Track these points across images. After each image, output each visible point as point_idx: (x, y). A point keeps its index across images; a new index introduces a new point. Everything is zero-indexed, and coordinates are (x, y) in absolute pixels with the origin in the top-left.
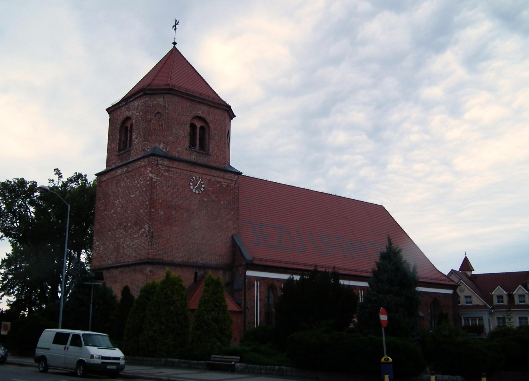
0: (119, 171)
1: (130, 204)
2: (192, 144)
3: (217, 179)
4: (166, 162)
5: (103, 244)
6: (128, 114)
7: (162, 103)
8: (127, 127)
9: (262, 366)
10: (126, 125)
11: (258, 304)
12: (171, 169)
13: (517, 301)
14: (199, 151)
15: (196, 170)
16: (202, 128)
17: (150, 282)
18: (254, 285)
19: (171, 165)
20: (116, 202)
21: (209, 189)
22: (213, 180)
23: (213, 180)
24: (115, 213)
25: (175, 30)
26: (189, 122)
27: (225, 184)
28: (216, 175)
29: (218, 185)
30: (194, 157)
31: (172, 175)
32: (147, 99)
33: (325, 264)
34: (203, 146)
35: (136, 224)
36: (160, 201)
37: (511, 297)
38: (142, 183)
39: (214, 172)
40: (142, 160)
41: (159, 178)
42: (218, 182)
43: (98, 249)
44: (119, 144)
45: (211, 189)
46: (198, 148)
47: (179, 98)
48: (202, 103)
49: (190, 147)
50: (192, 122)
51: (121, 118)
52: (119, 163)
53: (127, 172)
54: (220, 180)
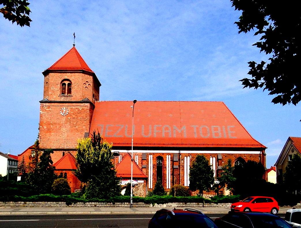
2: (63, 93)
4: (47, 104)
15: (64, 105)
19: (50, 105)
21: (72, 112)
23: (73, 108)
29: (77, 110)
30: (62, 99)
36: (45, 122)
39: (74, 104)
41: (44, 112)
42: (77, 108)
54: (78, 107)
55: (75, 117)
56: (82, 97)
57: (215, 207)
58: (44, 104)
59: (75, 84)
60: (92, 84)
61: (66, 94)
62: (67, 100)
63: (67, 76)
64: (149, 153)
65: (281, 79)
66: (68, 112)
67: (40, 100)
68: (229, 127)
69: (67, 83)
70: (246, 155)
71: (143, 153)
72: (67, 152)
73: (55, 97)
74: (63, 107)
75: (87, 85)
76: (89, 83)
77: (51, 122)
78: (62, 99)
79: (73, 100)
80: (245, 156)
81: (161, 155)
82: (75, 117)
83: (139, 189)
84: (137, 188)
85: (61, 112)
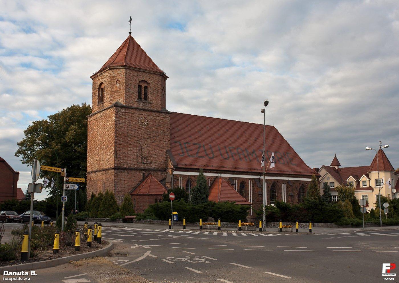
0: (99, 115)
1: (105, 135)
2: (139, 97)
3: (156, 118)
4: (123, 110)
5: (92, 158)
6: (102, 80)
7: (41, 147)
8: (102, 88)
10: (101, 87)
11: (277, 176)
12: (127, 114)
13: (361, 185)
16: (146, 87)
18: (179, 180)
20: (98, 134)
21: (151, 124)
22: (153, 118)
23: (153, 118)
24: (98, 140)
25: (130, 24)
26: (137, 84)
27: (161, 120)
30: (140, 106)
32: (111, 72)
34: (146, 98)
35: (108, 146)
36: (121, 133)
37: (358, 182)
38: (110, 122)
40: (110, 109)
43: (90, 161)
44: (99, 99)
45: (152, 124)
46: (143, 99)
47: (130, 70)
48: (145, 72)
49: (138, 99)
50: (139, 84)
51: (99, 83)
52: (98, 110)
53: (102, 116)
54: (158, 118)
55: (156, 130)
65: (385, 267)
71: (229, 178)
73: (132, 101)
74: (142, 116)
82: (156, 130)
85: (139, 121)
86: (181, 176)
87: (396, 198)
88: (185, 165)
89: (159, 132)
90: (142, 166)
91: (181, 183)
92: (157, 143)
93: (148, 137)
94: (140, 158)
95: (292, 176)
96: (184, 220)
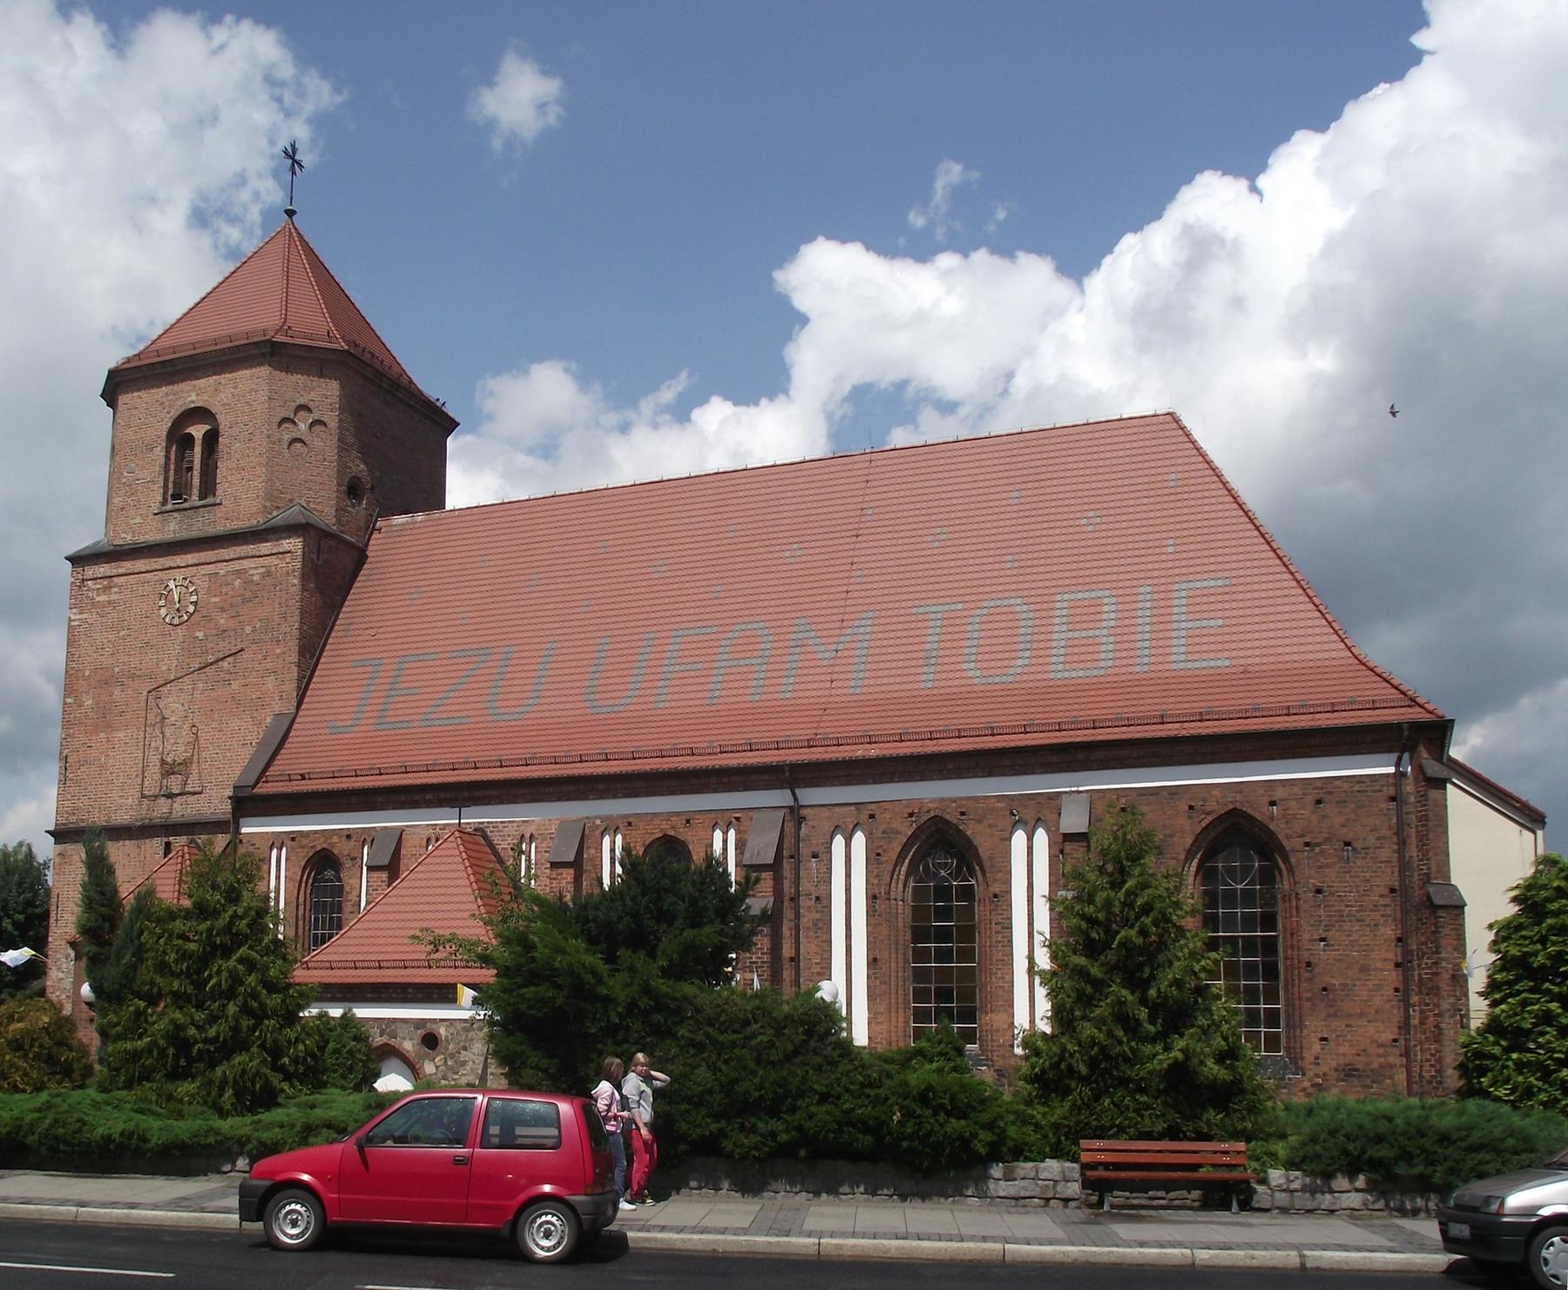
4: (103, 569)
9: (1546, 1086)
14: (202, 503)
17: (343, 860)
19: (114, 572)
23: (222, 572)
28: (232, 556)
29: (237, 583)
30: (173, 529)
31: (117, 597)
33: (565, 748)
36: (87, 673)
54: (246, 563)
55: (232, 624)
56: (268, 504)
57: (1267, 1210)
58: (90, 572)
59: (235, 431)
60: (332, 419)
61: (195, 499)
62: (194, 533)
63: (192, 393)
64: (603, 819)
66: (194, 598)
67: (73, 549)
68: (1063, 601)
69: (198, 431)
70: (1279, 793)
72: (184, 839)
73: (138, 520)
75: (303, 426)
76: (316, 415)
77: (117, 669)
78: (172, 526)
79: (221, 528)
80: (1273, 803)
81: (673, 828)
82: (232, 624)
83: (464, 1063)
84: (452, 1056)
86: (278, 841)
87: (789, 791)
88: (303, 778)
89: (248, 629)
90: (161, 810)
91: (278, 877)
92: (235, 685)
93: (197, 666)
94: (154, 770)
95: (480, 794)
96: (1517, 1199)
